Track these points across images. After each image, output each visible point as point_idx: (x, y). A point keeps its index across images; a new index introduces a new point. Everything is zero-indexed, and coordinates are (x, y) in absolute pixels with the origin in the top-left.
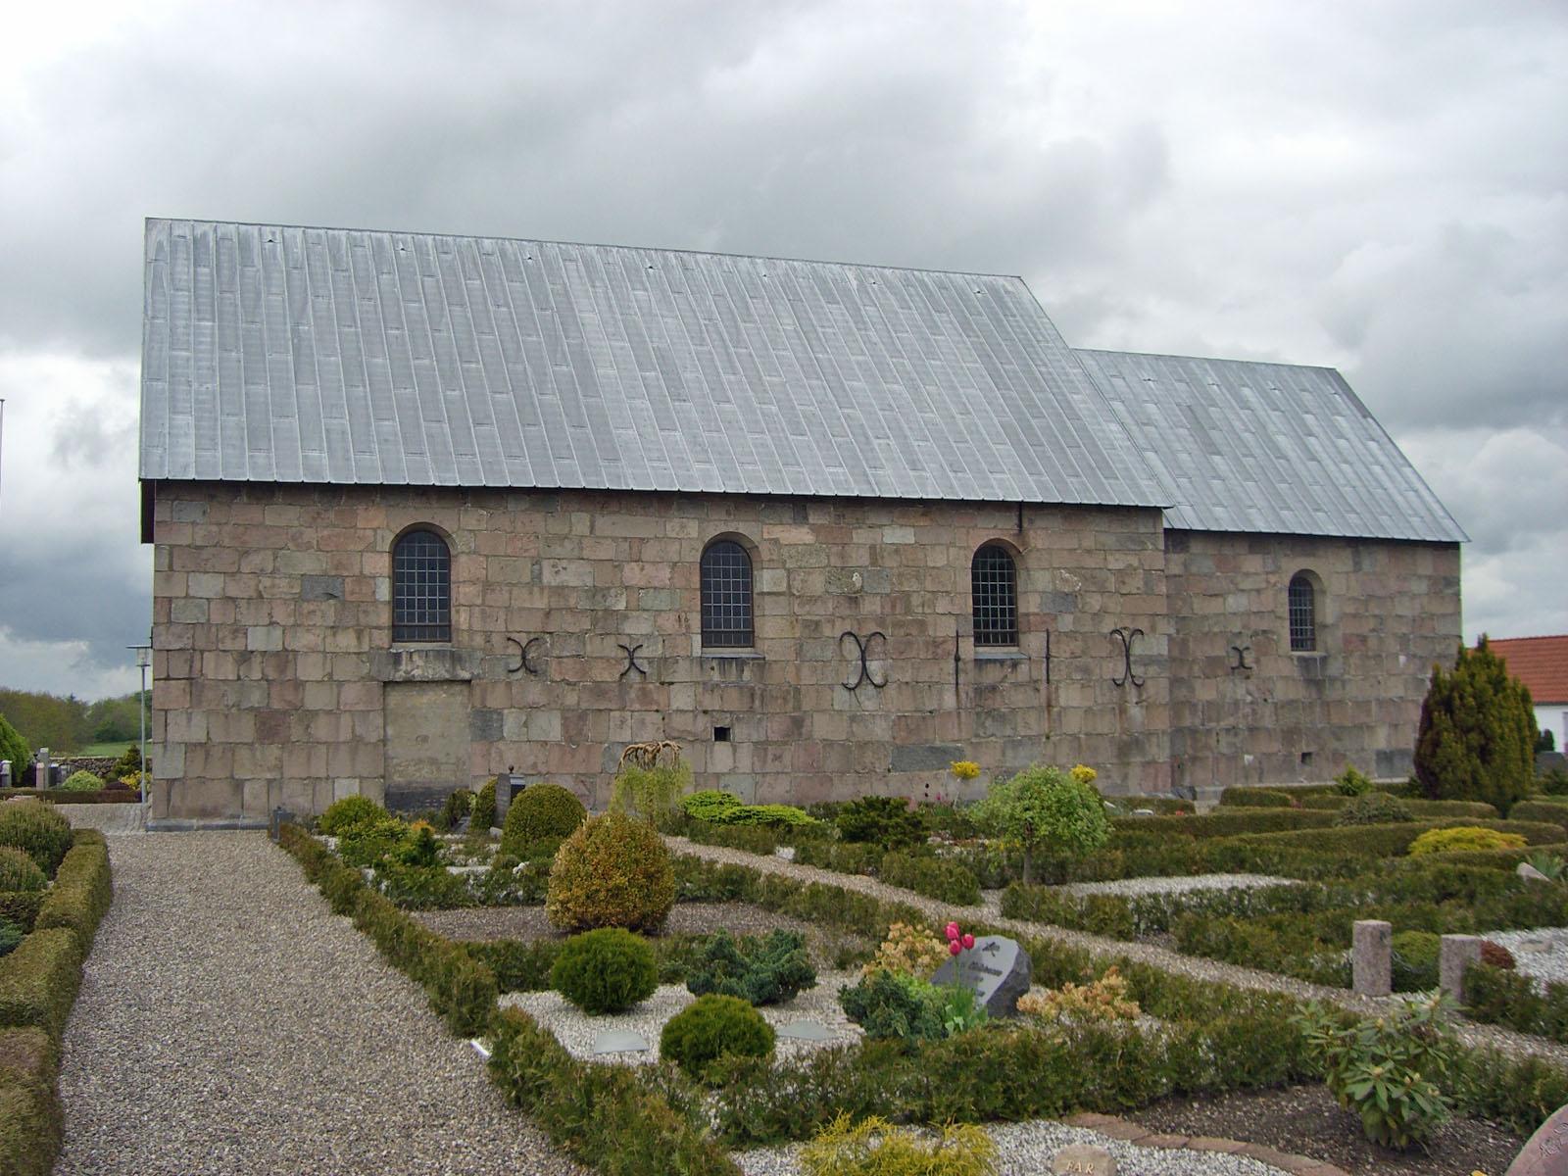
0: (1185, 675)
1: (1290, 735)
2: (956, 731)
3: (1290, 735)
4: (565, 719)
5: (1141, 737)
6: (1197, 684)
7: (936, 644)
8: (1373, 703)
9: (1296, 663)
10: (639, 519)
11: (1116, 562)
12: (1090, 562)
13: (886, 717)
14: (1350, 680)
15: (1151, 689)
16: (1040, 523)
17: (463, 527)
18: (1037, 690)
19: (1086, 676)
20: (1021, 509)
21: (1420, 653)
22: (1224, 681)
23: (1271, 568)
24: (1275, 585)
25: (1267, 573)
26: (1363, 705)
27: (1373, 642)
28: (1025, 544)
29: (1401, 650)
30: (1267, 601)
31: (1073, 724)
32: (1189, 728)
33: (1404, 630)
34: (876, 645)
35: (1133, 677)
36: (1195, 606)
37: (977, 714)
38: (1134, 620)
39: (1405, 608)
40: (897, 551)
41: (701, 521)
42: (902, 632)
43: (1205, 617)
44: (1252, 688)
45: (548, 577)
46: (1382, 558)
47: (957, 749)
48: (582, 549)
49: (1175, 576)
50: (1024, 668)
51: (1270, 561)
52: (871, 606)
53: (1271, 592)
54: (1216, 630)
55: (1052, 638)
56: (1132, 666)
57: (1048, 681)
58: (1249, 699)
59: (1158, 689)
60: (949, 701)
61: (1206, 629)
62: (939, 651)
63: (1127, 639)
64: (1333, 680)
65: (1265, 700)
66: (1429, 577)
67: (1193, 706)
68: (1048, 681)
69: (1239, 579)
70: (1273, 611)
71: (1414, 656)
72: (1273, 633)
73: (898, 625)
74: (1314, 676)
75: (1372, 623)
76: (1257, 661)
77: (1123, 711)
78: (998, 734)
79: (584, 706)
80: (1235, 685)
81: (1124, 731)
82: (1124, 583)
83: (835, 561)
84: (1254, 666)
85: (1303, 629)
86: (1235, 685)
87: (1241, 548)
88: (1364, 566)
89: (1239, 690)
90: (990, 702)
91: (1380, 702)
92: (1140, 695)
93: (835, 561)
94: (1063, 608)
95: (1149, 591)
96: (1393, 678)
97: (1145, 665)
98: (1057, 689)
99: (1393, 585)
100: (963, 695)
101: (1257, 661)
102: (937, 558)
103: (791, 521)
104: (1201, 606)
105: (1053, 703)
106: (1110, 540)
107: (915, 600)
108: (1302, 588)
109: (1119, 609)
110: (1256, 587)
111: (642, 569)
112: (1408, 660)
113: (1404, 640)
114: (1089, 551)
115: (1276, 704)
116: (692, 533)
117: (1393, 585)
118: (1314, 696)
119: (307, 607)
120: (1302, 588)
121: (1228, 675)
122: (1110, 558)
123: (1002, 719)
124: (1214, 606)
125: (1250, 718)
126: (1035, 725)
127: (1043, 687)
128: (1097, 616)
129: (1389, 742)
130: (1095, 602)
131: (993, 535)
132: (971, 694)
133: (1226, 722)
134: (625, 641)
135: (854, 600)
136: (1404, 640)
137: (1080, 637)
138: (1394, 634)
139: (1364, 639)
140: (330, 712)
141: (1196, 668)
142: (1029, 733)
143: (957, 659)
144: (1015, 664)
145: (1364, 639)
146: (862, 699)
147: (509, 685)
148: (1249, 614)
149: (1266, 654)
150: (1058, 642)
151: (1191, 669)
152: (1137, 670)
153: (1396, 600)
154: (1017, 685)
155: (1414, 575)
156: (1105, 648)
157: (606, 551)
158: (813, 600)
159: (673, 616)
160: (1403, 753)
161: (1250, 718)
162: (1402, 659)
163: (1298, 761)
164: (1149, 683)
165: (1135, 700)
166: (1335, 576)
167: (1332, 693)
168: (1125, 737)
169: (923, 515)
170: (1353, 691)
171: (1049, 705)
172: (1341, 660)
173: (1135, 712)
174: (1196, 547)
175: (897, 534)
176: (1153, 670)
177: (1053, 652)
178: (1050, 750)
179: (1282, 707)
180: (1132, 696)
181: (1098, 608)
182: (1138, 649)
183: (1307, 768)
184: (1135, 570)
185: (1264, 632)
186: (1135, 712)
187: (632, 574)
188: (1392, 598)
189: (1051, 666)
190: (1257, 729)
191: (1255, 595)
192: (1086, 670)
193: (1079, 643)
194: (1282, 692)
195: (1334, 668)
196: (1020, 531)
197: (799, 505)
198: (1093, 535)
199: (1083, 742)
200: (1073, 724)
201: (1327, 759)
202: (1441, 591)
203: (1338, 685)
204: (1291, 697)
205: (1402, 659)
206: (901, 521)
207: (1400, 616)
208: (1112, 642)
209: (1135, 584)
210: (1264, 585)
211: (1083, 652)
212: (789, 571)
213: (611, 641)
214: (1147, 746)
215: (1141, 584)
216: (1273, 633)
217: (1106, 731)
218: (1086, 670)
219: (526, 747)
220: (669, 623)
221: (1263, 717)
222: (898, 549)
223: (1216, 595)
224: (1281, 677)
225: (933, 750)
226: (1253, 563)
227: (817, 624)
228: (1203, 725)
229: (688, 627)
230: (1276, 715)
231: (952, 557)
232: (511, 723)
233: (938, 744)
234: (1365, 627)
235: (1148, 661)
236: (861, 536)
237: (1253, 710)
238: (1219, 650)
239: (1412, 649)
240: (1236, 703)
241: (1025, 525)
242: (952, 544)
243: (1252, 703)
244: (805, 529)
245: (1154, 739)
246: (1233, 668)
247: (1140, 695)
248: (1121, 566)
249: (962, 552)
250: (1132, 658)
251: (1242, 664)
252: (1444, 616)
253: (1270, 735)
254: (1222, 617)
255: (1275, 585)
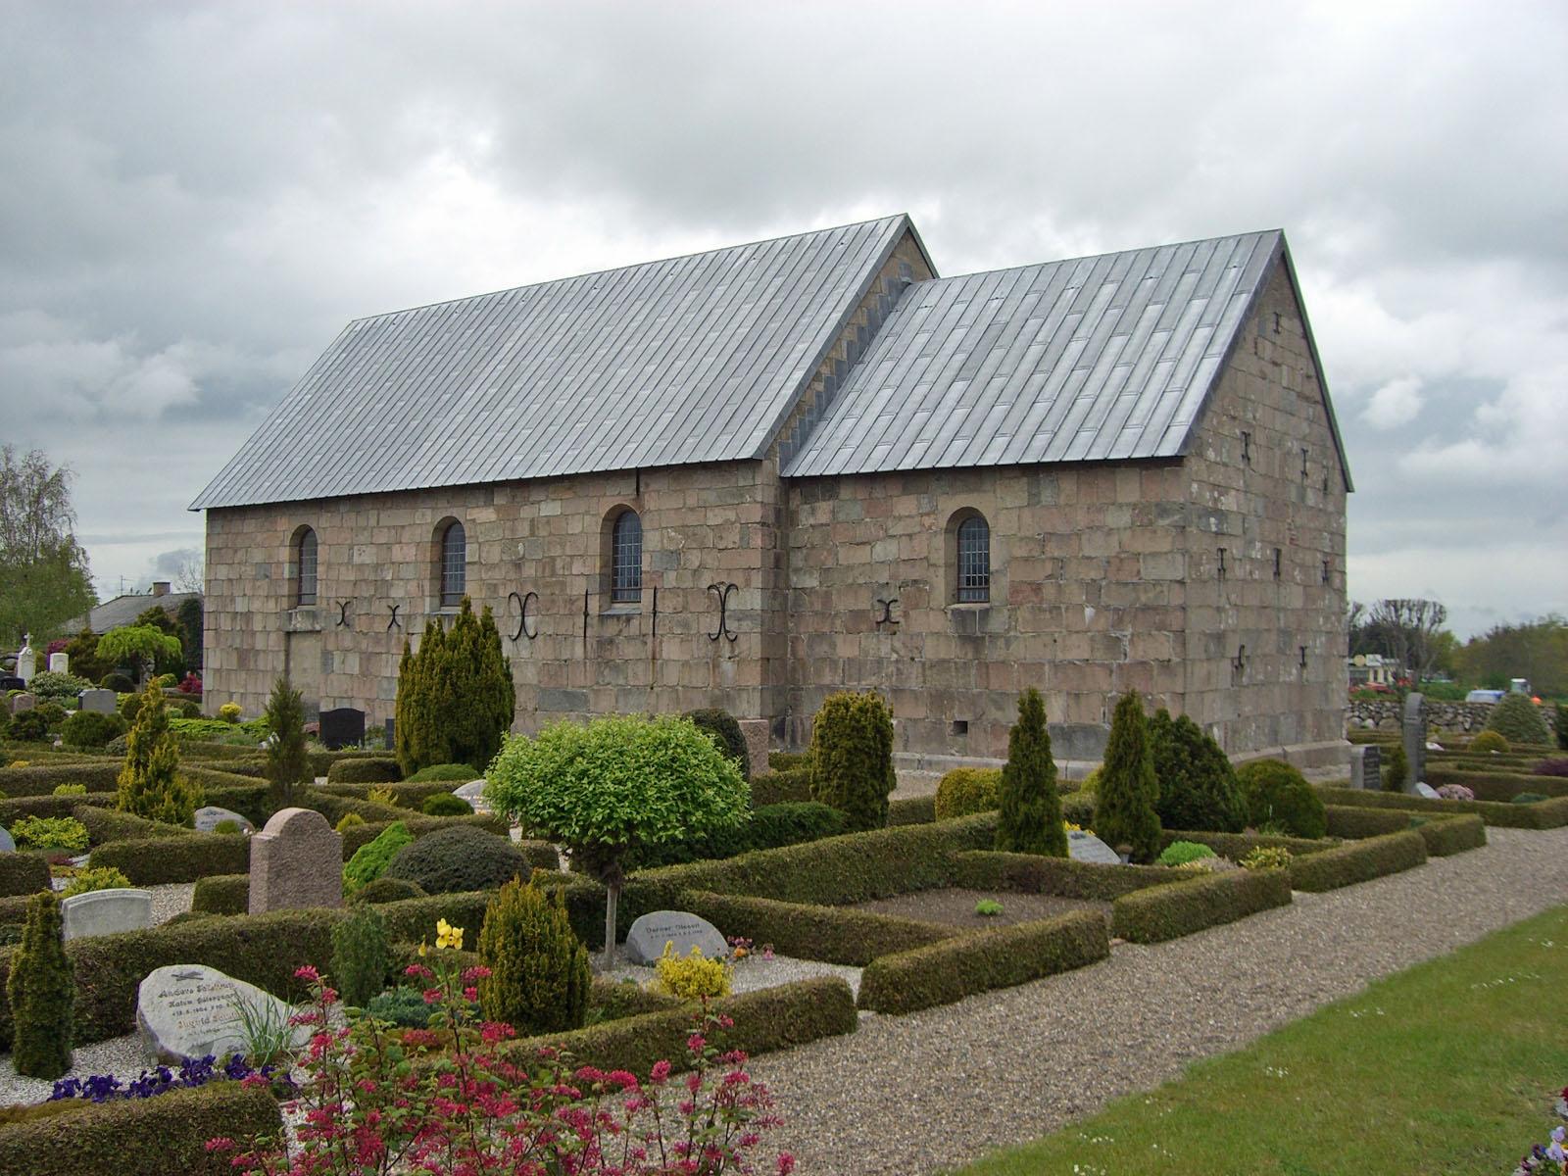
0: (826, 629)
1: (940, 699)
2: (583, 678)
3: (940, 699)
4: (361, 659)
5: (732, 692)
6: (839, 640)
7: (572, 602)
8: (1047, 667)
9: (949, 615)
10: (401, 512)
11: (715, 518)
12: (692, 519)
13: (534, 664)
14: (1016, 637)
15: (743, 645)
16: (654, 486)
17: (323, 525)
18: (646, 643)
19: (685, 631)
20: (638, 473)
21: (1115, 604)
22: (867, 637)
23: (926, 508)
24: (930, 528)
25: (922, 515)
26: (1034, 668)
27: (1049, 592)
28: (641, 507)
29: (1087, 601)
30: (920, 547)
31: (672, 676)
32: (828, 686)
33: (1093, 575)
34: (532, 604)
35: (727, 632)
36: (840, 556)
37: (599, 663)
38: (729, 574)
39: (1097, 547)
40: (548, 522)
41: (433, 509)
42: (548, 592)
43: (850, 568)
44: (898, 645)
45: (357, 559)
46: (1068, 485)
47: (583, 694)
48: (372, 536)
49: (822, 525)
50: (635, 622)
51: (926, 500)
52: (529, 570)
53: (924, 536)
54: (861, 581)
55: (658, 595)
56: (727, 621)
57: (654, 634)
58: (895, 656)
59: (752, 645)
60: (579, 651)
61: (850, 581)
62: (574, 608)
63: (723, 595)
64: (993, 637)
65: (913, 659)
66: (1134, 506)
67: (834, 663)
68: (654, 634)
69: (890, 523)
70: (926, 558)
71: (1107, 608)
72: (926, 583)
73: (547, 585)
74: (971, 634)
75: (1049, 568)
76: (906, 615)
77: (716, 666)
78: (613, 682)
79: (370, 650)
80: (879, 641)
81: (718, 686)
82: (721, 538)
83: (508, 534)
84: (902, 620)
85: (973, 579)
86: (879, 641)
87: (894, 489)
88: (1043, 498)
89: (883, 646)
90: (608, 653)
91: (1056, 666)
92: (733, 651)
93: (508, 534)
94: (668, 566)
95: (745, 545)
96: (1074, 636)
97: (739, 620)
98: (661, 642)
99: (1081, 519)
100: (589, 646)
101: (906, 615)
102: (575, 527)
103: (446, 505)
104: (847, 556)
105: (658, 656)
106: (711, 497)
107: (559, 564)
108: (968, 526)
109: (716, 564)
110: (909, 531)
111: (401, 549)
112: (1096, 613)
113: (1093, 589)
114: (692, 509)
115: (924, 664)
116: (427, 518)
117: (1081, 519)
118: (970, 656)
119: (258, 584)
120: (968, 526)
121: (872, 630)
122: (710, 514)
123: (616, 669)
124: (862, 555)
125: (894, 679)
126: (640, 675)
127: (650, 639)
128: (696, 572)
129: (1067, 715)
130: (694, 559)
131: (617, 501)
132: (595, 646)
133: (868, 682)
134: (391, 603)
135: (518, 565)
136: (1093, 589)
137: (681, 593)
138: (1081, 582)
139: (1037, 588)
140: (264, 651)
141: (838, 622)
142: (637, 683)
143: (586, 615)
144: (629, 618)
145: (1037, 588)
146: (520, 648)
147: (337, 634)
148: (897, 562)
149: (916, 607)
150: (663, 598)
151: (833, 623)
152: (731, 625)
153: (1084, 538)
154: (629, 638)
155: (1113, 504)
156: (702, 603)
157: (382, 538)
158: (493, 566)
159: (415, 583)
160: (1088, 731)
161: (894, 679)
162: (1089, 612)
163: (949, 730)
164: (741, 637)
165: (728, 655)
166: (1005, 513)
167: (994, 653)
168: (717, 691)
169: (569, 489)
170: (1018, 651)
171: (654, 658)
172: (1006, 613)
173: (728, 667)
174: (845, 493)
175: (550, 508)
176: (746, 625)
177: (658, 609)
178: (653, 701)
179: (932, 666)
180: (726, 649)
181: (697, 564)
182: (732, 604)
183: (960, 739)
184: (733, 523)
185: (915, 582)
186: (728, 667)
187: (397, 554)
188: (1078, 535)
189: (657, 621)
190: (902, 690)
191: (915, 535)
192: (686, 625)
193: (680, 599)
194: (932, 650)
195: (996, 624)
196: (638, 494)
197: (486, 490)
198: (697, 493)
199: (681, 694)
200: (672, 676)
201: (985, 731)
202: (1151, 524)
203: (1001, 643)
204: (942, 656)
205: (1089, 612)
206: (553, 496)
207: (1089, 558)
208: (710, 597)
209: (732, 538)
210: (917, 529)
211: (684, 608)
212: (480, 544)
213: (384, 603)
214: (737, 702)
215: (737, 539)
216: (926, 583)
217: (700, 685)
218: (686, 625)
219: (343, 677)
220: (412, 587)
221: (908, 678)
222: (548, 520)
223: (863, 543)
224: (933, 634)
225: (566, 693)
226: (906, 505)
227: (495, 585)
228: (843, 683)
229: (423, 591)
230: (924, 676)
231: (582, 524)
232: (337, 658)
233: (570, 689)
234: (1039, 574)
235: (742, 616)
236: (526, 512)
237: (898, 669)
238: (864, 602)
239: (1104, 600)
240: (879, 661)
241: (641, 490)
242: (587, 513)
243: (897, 661)
244: (491, 510)
245: (744, 695)
246: (878, 623)
247: (733, 651)
248: (719, 521)
249: (594, 519)
250: (727, 613)
251: (887, 619)
252: (1154, 555)
253: (916, 698)
254: (868, 567)
255: (930, 528)
